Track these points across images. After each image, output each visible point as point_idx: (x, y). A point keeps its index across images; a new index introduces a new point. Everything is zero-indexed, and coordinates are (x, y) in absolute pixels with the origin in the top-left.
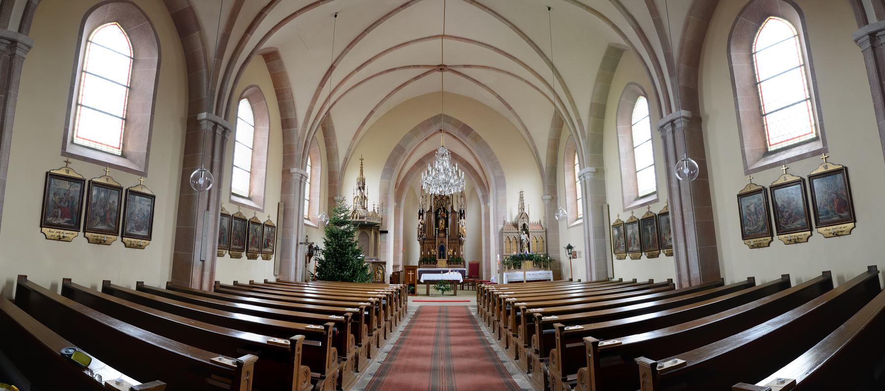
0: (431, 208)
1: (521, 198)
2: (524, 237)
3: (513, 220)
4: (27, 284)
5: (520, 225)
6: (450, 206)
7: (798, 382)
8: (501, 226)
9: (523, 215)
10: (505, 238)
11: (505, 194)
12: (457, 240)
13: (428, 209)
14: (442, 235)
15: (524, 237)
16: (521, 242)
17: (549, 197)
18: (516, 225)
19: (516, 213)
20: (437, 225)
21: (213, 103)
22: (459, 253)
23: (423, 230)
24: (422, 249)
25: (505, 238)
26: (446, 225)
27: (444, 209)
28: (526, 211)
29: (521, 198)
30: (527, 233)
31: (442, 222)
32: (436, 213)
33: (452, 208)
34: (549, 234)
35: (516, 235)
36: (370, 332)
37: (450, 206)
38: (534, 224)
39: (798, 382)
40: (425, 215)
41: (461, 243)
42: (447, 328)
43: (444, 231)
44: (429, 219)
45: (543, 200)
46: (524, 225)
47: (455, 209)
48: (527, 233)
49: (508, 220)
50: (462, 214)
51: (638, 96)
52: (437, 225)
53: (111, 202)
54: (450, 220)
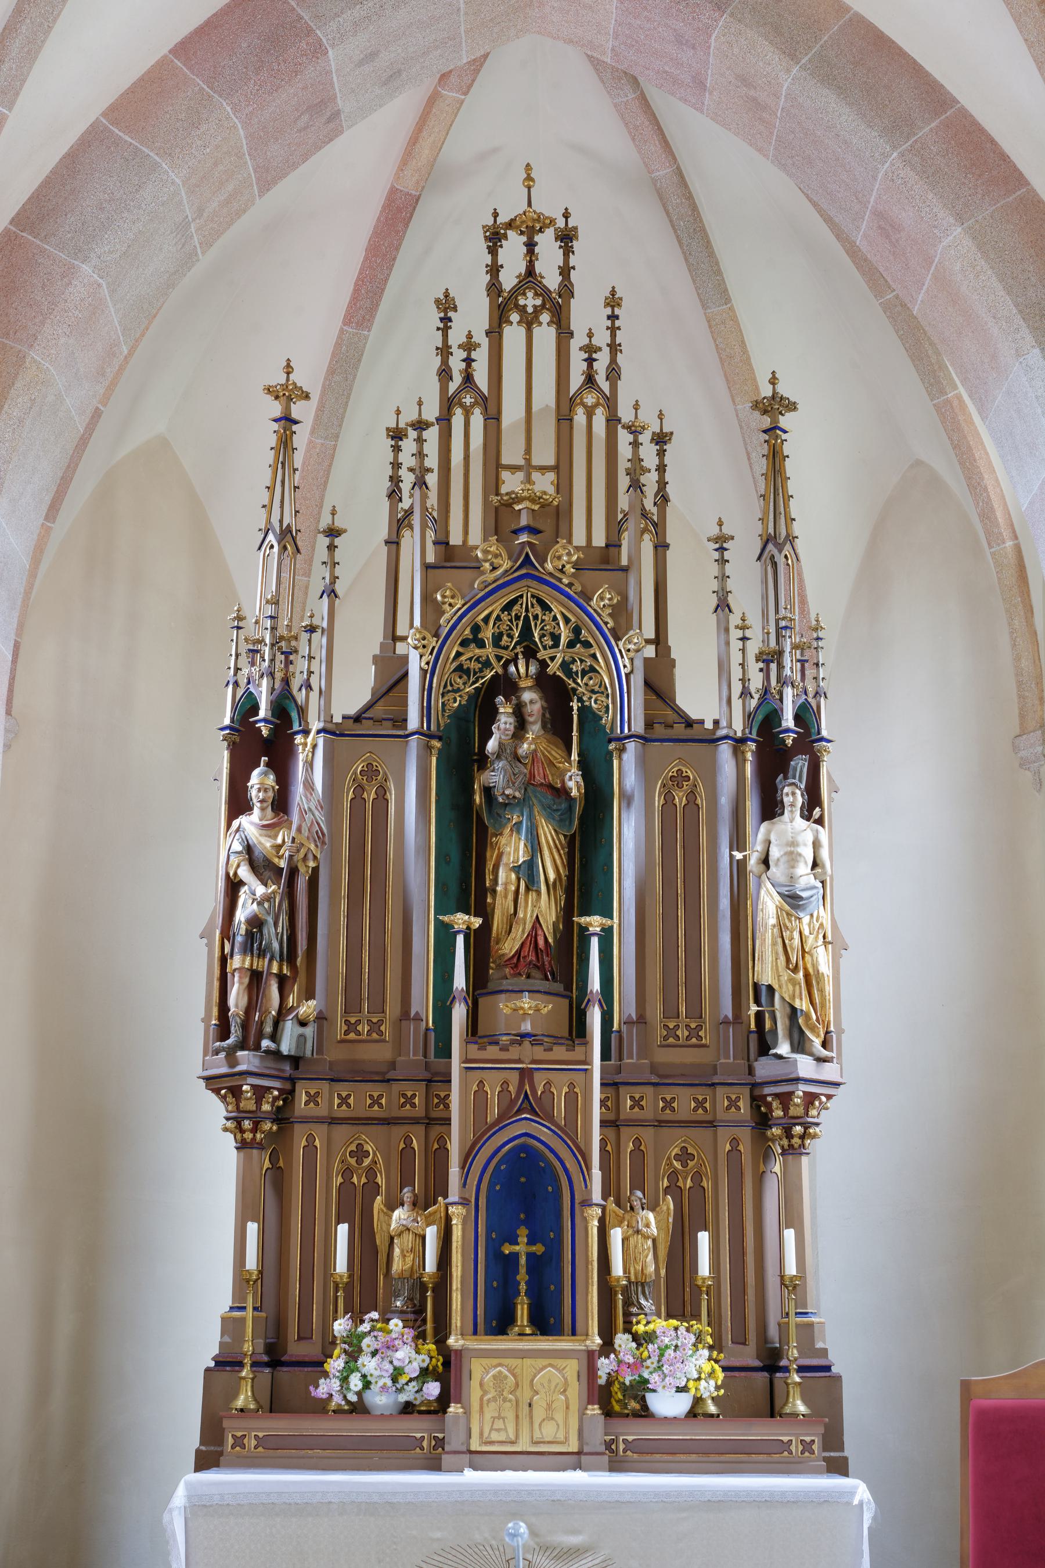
0: (392, 684)
6: (632, 653)
12: (738, 1084)
13: (353, 691)
14: (526, 1008)
20: (466, 880)
21: (579, 881)
22: (745, 1254)
23: (278, 944)
24: (272, 1190)
26: (585, 881)
27: (556, 692)
31: (523, 850)
32: (461, 750)
33: (659, 686)
36: (247, 708)
37: (632, 653)
40: (311, 760)
41: (777, 1121)
42: (237, 655)
43: (559, 961)
44: (365, 816)
47: (698, 697)
50: (783, 755)
52: (466, 880)
54: (629, 835)
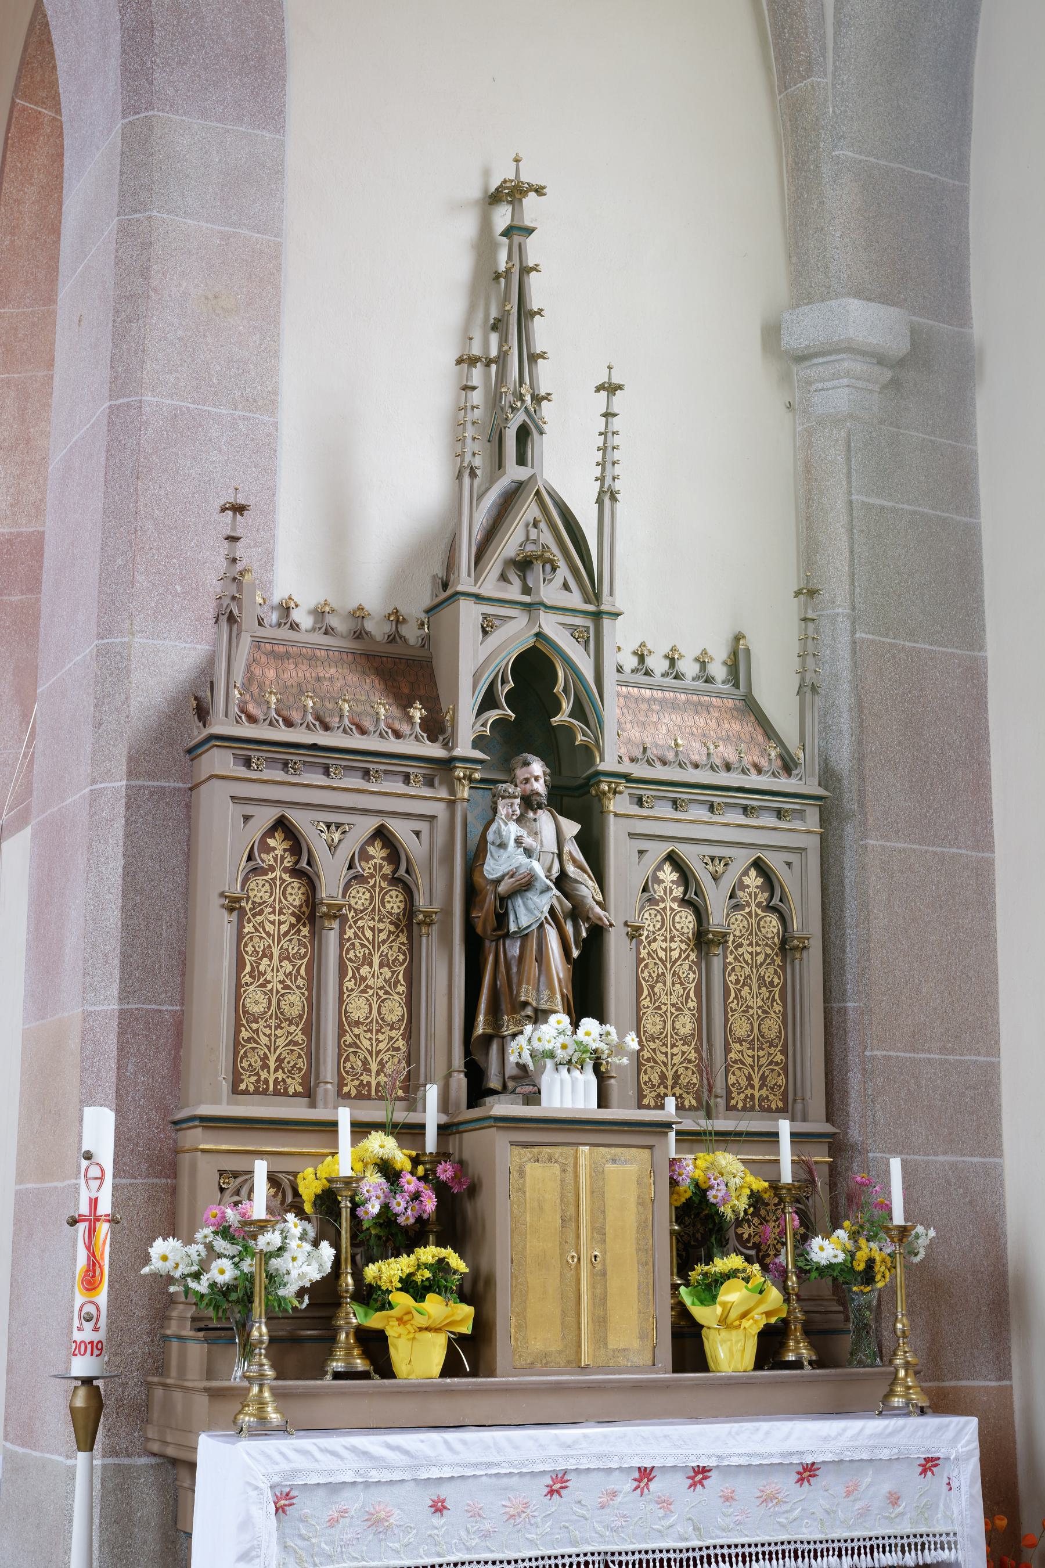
1: (504, 302)
2: (529, 845)
3: (371, 583)
4: (469, 1207)
5: (477, 656)
7: (160, 1239)
8: (169, 654)
9: (511, 517)
10: (227, 833)
11: (256, 183)
15: (529, 845)
16: (485, 926)
17: (868, 322)
18: (403, 665)
19: (405, 481)
25: (227, 833)
28: (564, 467)
29: (504, 302)
30: (577, 796)
34: (876, 850)
35: (416, 813)
38: (660, 673)
39: (160, 1239)
45: (788, 357)
46: (534, 668)
48: (577, 796)
49: (293, 577)
51: (553, 728)
53: (326, 1251)
